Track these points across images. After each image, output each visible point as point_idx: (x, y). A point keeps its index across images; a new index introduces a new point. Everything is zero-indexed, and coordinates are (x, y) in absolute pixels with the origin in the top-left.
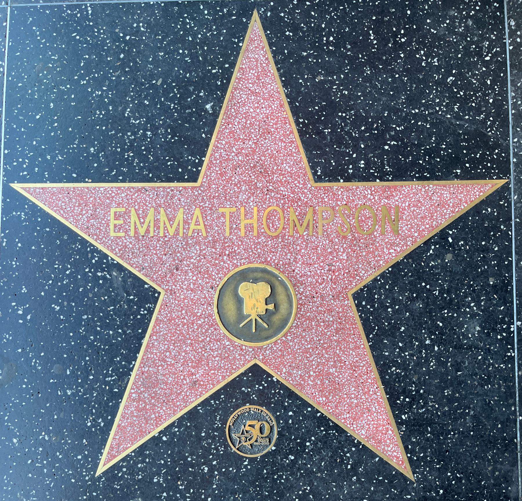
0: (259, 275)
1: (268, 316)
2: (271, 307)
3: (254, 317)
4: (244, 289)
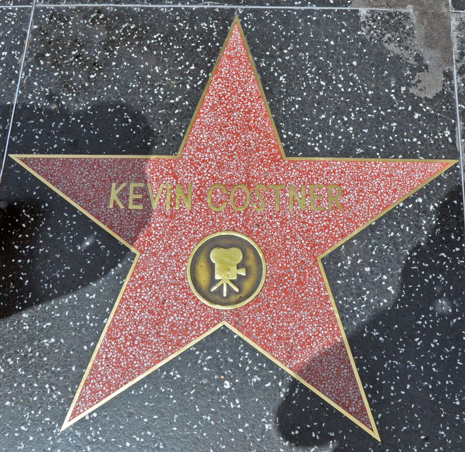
0: (227, 242)
1: (239, 281)
2: (243, 273)
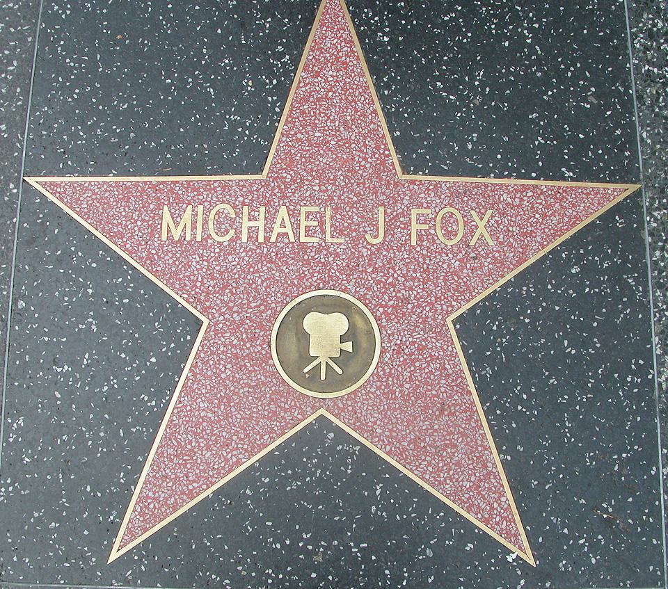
1: (343, 359)
2: (348, 346)
3: (322, 360)
4: (311, 322)
